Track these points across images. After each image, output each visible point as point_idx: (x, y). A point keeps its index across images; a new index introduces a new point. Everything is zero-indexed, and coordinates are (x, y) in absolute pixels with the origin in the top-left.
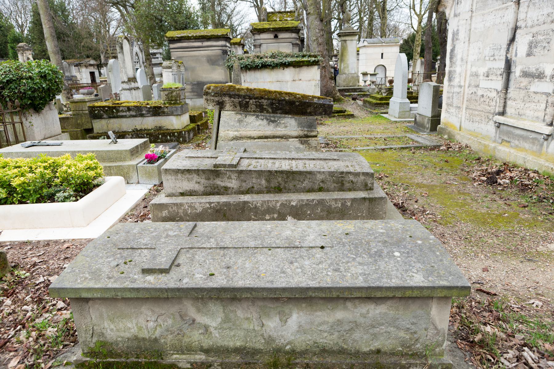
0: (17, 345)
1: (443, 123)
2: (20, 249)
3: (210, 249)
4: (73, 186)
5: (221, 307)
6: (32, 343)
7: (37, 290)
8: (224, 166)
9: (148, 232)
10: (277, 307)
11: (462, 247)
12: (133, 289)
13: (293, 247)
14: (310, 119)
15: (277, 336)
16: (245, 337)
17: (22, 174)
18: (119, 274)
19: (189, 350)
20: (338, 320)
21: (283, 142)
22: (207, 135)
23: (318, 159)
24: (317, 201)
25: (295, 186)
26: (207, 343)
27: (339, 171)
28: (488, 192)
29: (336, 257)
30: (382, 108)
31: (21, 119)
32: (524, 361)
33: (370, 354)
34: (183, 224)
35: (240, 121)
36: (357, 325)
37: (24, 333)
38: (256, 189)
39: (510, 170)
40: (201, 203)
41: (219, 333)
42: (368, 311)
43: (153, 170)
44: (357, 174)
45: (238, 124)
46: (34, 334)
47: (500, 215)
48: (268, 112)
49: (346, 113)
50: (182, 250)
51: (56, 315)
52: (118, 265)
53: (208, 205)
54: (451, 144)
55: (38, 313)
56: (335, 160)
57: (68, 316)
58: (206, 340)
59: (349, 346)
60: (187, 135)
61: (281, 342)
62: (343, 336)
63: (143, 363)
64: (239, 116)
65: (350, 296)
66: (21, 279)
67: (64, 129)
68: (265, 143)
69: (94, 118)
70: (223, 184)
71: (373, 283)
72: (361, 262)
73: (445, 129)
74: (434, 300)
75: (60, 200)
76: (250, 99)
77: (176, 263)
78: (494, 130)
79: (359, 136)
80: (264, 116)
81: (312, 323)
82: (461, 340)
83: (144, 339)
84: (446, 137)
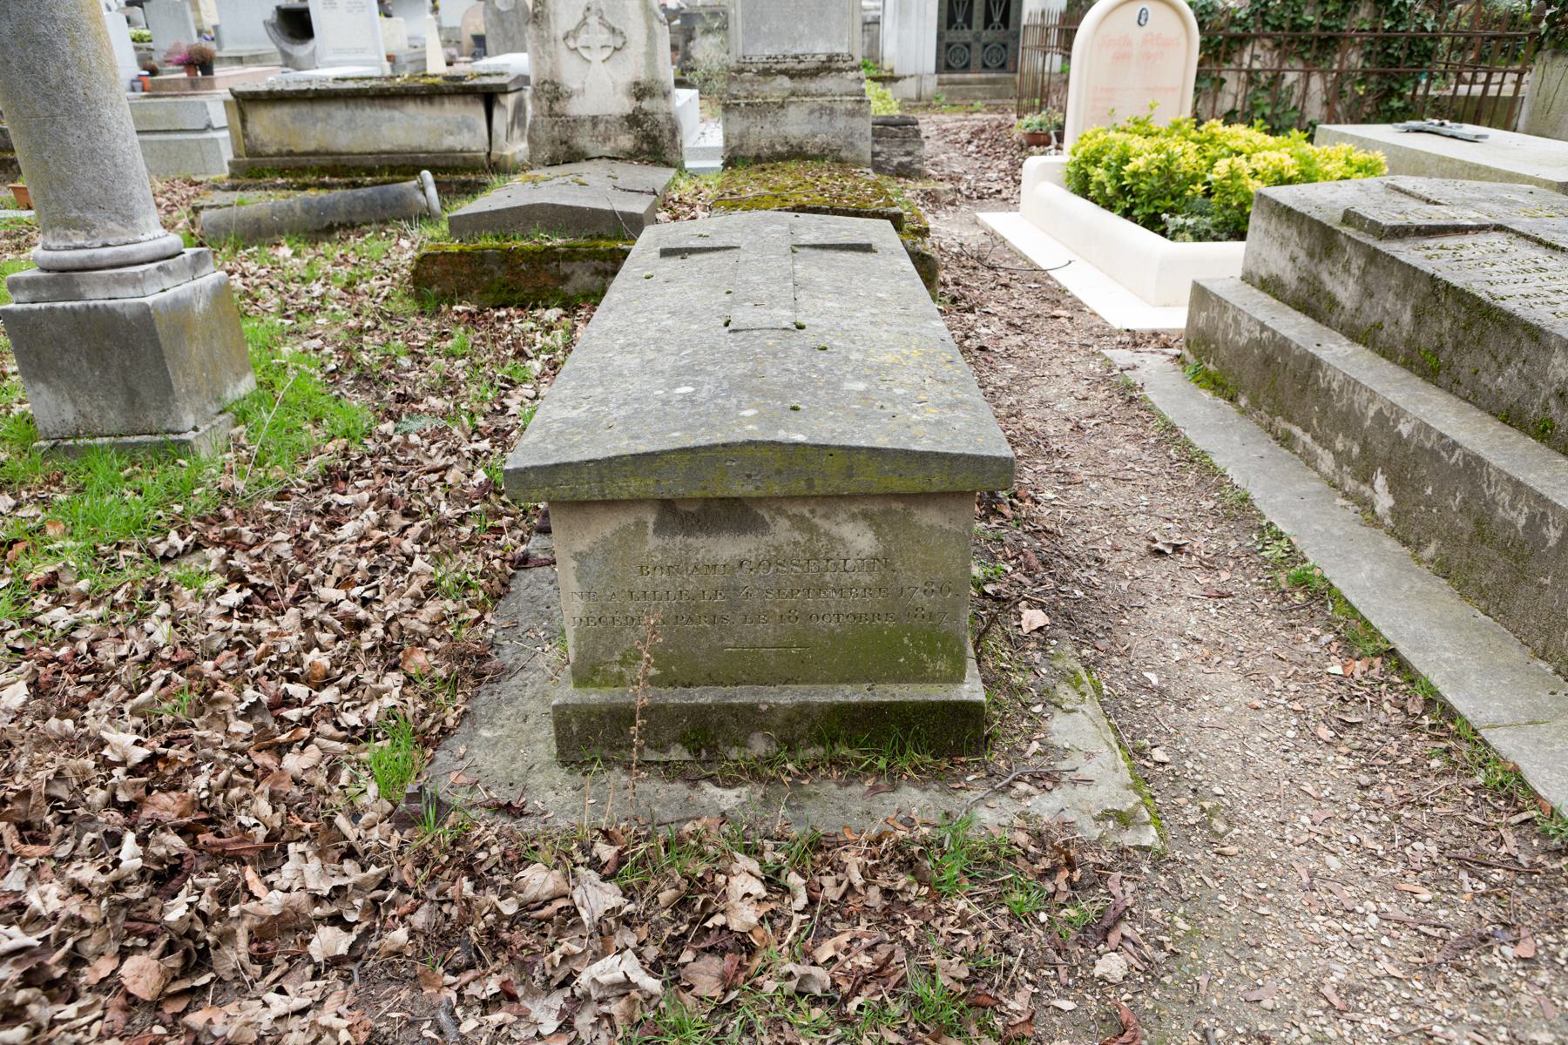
24: (1465, 455)
38: (1383, 335)
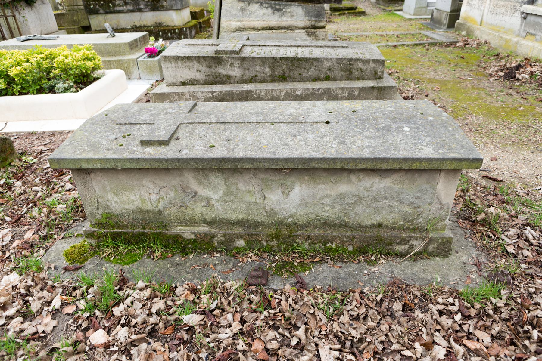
0: (31, 220)
1: (463, 18)
2: (27, 138)
3: (210, 123)
4: (72, 77)
5: (223, 180)
6: (44, 218)
7: (46, 174)
8: (226, 52)
9: (146, 111)
10: (279, 179)
11: (472, 138)
12: (132, 159)
13: (297, 122)
14: (318, 7)
15: (280, 209)
16: (247, 210)
17: (18, 63)
18: (118, 146)
19: (192, 222)
20: (341, 194)
21: (289, 33)
22: (209, 34)
23: (325, 46)
25: (300, 74)
26: (209, 216)
27: (347, 57)
28: (505, 87)
29: (342, 131)
30: (396, 5)
31: (13, 13)
32: (525, 238)
33: (371, 227)
34: (182, 104)
35: (243, 10)
36: (360, 198)
37: (36, 210)
38: (259, 77)
39: (531, 65)
40: (203, 92)
41: (221, 205)
42: (372, 185)
43: (154, 65)
44: (367, 62)
45: (241, 13)
46: (45, 210)
47: (516, 109)
49: (357, 10)
50: (181, 125)
51: (65, 194)
52: (116, 139)
53: (210, 95)
54: (469, 40)
55: (48, 193)
56: (344, 47)
57: (76, 196)
58: (209, 213)
59: (351, 219)
60: (188, 32)
61: (281, 215)
62: (345, 209)
63: (149, 233)
65: (354, 168)
66: (29, 164)
67: (61, 27)
69: (90, 14)
70: (225, 72)
71: (380, 155)
72: (368, 135)
73: (463, 24)
74: (443, 174)
75: (60, 91)
77: (175, 137)
78: (519, 23)
79: (370, 33)
80: (268, 4)
81: (314, 196)
82: (462, 219)
83: (148, 211)
84: (464, 33)
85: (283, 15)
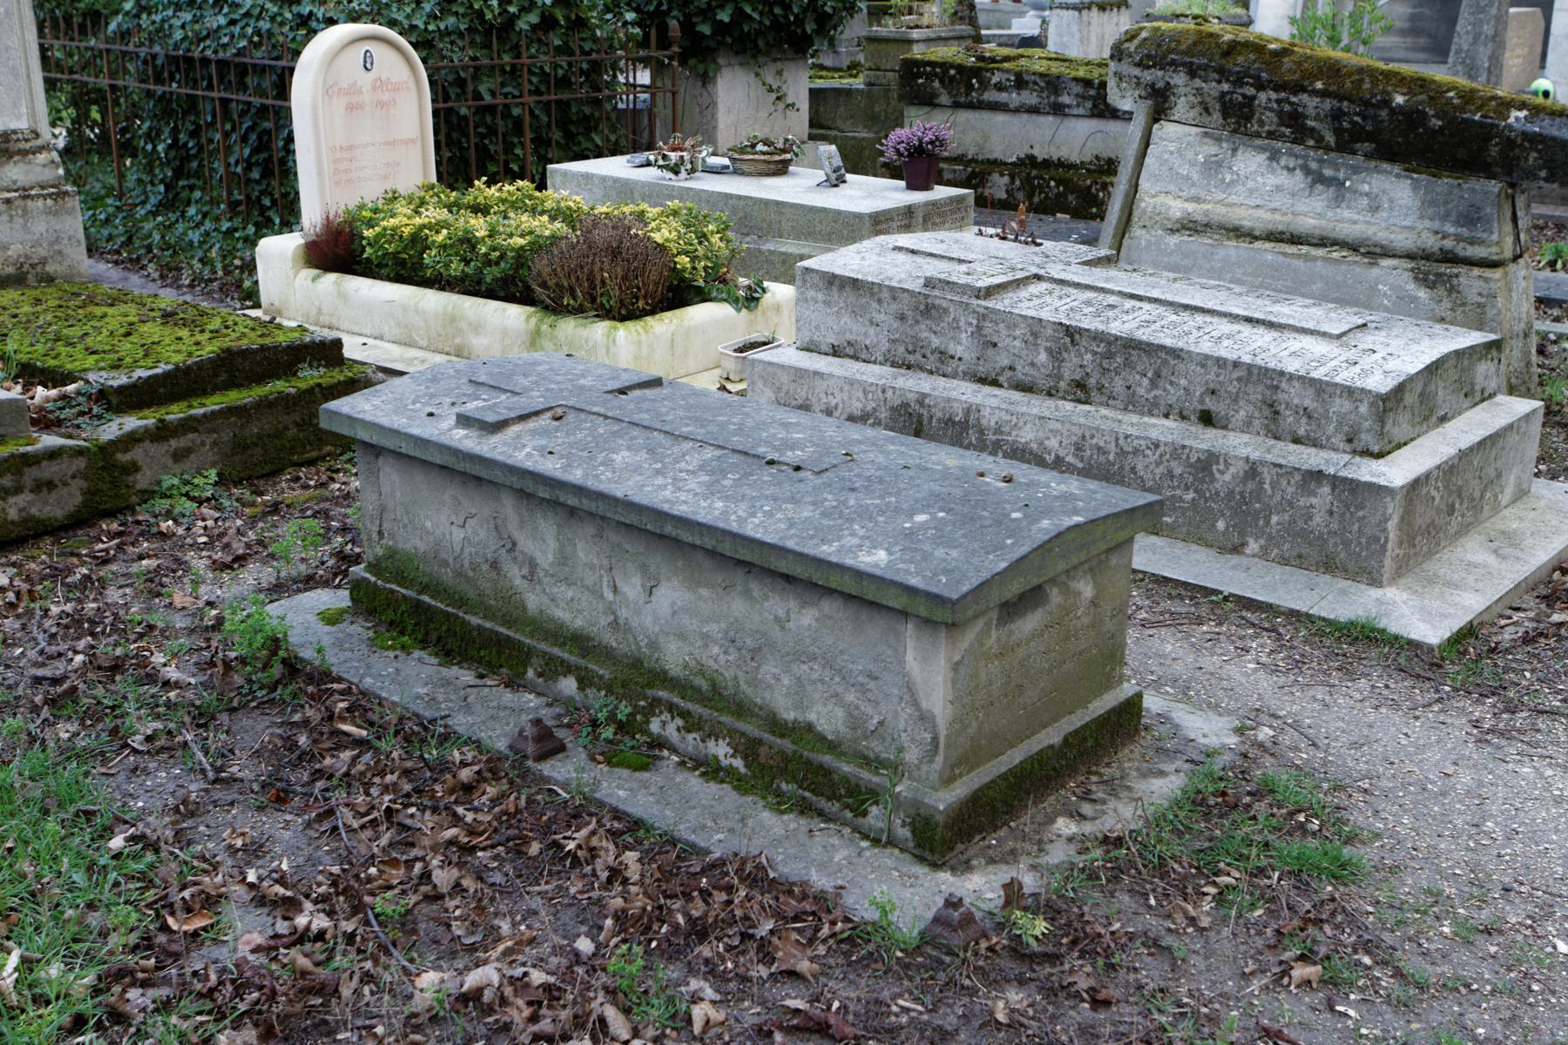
48: (1321, 144)
64: (1211, 149)
68: (1288, 260)
76: (1260, 87)
85: (1338, 200)
